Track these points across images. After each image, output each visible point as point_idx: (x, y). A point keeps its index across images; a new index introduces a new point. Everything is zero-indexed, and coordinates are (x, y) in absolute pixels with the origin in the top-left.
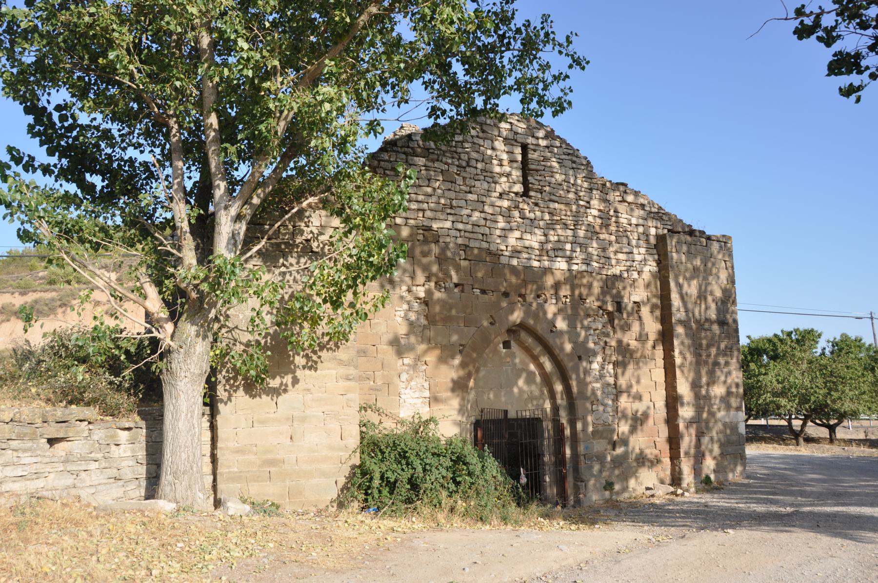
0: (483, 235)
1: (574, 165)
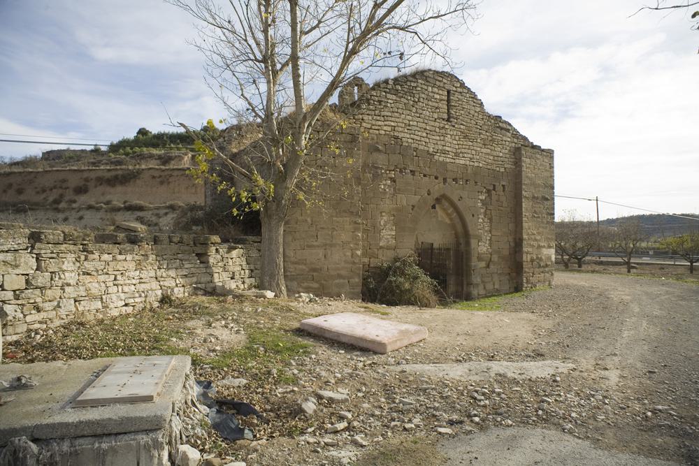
1: (475, 104)
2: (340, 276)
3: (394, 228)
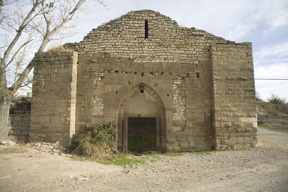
0: (127, 53)
1: (168, 24)
2: (58, 132)
3: (103, 105)
